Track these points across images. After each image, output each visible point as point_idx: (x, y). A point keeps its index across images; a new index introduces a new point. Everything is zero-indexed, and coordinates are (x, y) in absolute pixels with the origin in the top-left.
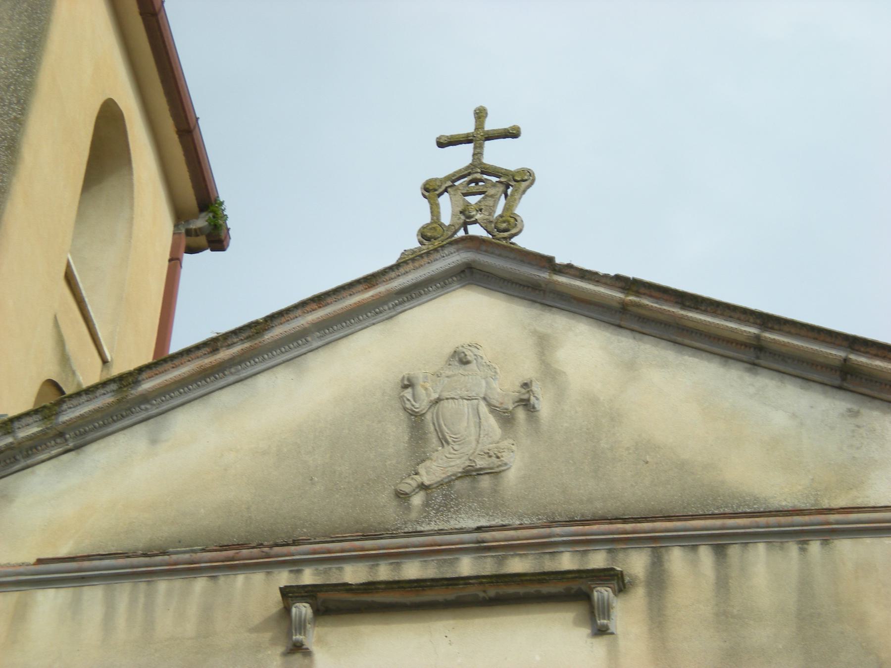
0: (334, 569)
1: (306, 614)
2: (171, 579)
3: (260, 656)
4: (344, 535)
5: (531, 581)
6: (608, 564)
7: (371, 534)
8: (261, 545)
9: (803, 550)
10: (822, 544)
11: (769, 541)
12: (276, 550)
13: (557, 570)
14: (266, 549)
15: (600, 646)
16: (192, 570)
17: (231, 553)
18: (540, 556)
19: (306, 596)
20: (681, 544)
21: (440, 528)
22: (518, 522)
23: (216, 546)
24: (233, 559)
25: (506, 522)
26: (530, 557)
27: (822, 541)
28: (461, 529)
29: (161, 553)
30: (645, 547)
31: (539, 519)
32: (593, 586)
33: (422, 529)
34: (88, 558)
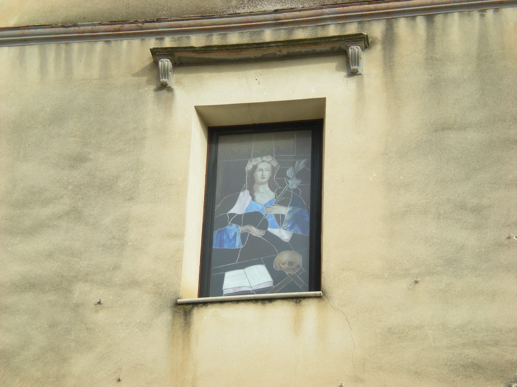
0: (184, 37)
1: (168, 66)
2: (81, 42)
3: (141, 91)
4: (189, 16)
5: (310, 44)
6: (359, 31)
7: (207, 15)
8: (136, 22)
9: (482, 16)
10: (494, 11)
11: (461, 11)
12: (147, 25)
13: (326, 36)
14: (140, 24)
15: (352, 82)
16: (93, 37)
17: (117, 26)
18: (315, 28)
19: (168, 55)
20: (405, 16)
21: (251, 11)
22: (301, 6)
23: (108, 22)
24: (119, 30)
25: (294, 6)
26: (309, 29)
27: (494, 9)
28: (265, 11)
29: (73, 25)
30: (383, 19)
31: (315, 4)
32: (348, 45)
33: (240, 12)
34: (27, 27)
